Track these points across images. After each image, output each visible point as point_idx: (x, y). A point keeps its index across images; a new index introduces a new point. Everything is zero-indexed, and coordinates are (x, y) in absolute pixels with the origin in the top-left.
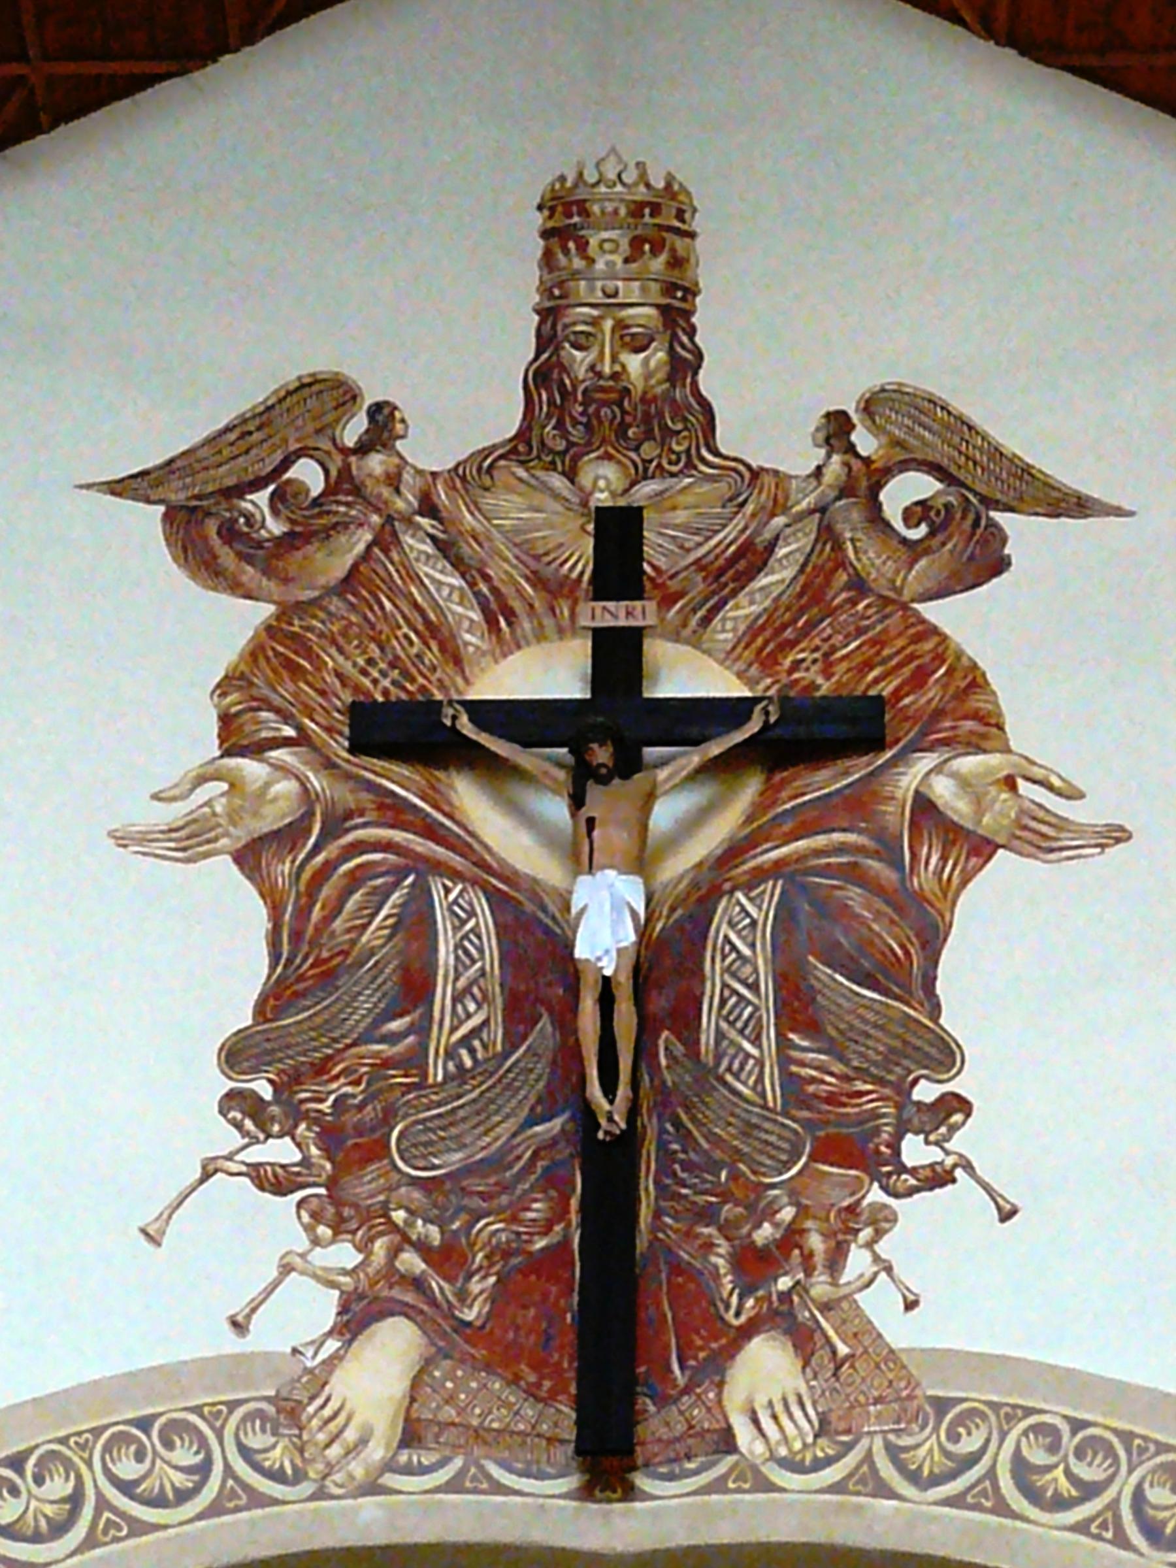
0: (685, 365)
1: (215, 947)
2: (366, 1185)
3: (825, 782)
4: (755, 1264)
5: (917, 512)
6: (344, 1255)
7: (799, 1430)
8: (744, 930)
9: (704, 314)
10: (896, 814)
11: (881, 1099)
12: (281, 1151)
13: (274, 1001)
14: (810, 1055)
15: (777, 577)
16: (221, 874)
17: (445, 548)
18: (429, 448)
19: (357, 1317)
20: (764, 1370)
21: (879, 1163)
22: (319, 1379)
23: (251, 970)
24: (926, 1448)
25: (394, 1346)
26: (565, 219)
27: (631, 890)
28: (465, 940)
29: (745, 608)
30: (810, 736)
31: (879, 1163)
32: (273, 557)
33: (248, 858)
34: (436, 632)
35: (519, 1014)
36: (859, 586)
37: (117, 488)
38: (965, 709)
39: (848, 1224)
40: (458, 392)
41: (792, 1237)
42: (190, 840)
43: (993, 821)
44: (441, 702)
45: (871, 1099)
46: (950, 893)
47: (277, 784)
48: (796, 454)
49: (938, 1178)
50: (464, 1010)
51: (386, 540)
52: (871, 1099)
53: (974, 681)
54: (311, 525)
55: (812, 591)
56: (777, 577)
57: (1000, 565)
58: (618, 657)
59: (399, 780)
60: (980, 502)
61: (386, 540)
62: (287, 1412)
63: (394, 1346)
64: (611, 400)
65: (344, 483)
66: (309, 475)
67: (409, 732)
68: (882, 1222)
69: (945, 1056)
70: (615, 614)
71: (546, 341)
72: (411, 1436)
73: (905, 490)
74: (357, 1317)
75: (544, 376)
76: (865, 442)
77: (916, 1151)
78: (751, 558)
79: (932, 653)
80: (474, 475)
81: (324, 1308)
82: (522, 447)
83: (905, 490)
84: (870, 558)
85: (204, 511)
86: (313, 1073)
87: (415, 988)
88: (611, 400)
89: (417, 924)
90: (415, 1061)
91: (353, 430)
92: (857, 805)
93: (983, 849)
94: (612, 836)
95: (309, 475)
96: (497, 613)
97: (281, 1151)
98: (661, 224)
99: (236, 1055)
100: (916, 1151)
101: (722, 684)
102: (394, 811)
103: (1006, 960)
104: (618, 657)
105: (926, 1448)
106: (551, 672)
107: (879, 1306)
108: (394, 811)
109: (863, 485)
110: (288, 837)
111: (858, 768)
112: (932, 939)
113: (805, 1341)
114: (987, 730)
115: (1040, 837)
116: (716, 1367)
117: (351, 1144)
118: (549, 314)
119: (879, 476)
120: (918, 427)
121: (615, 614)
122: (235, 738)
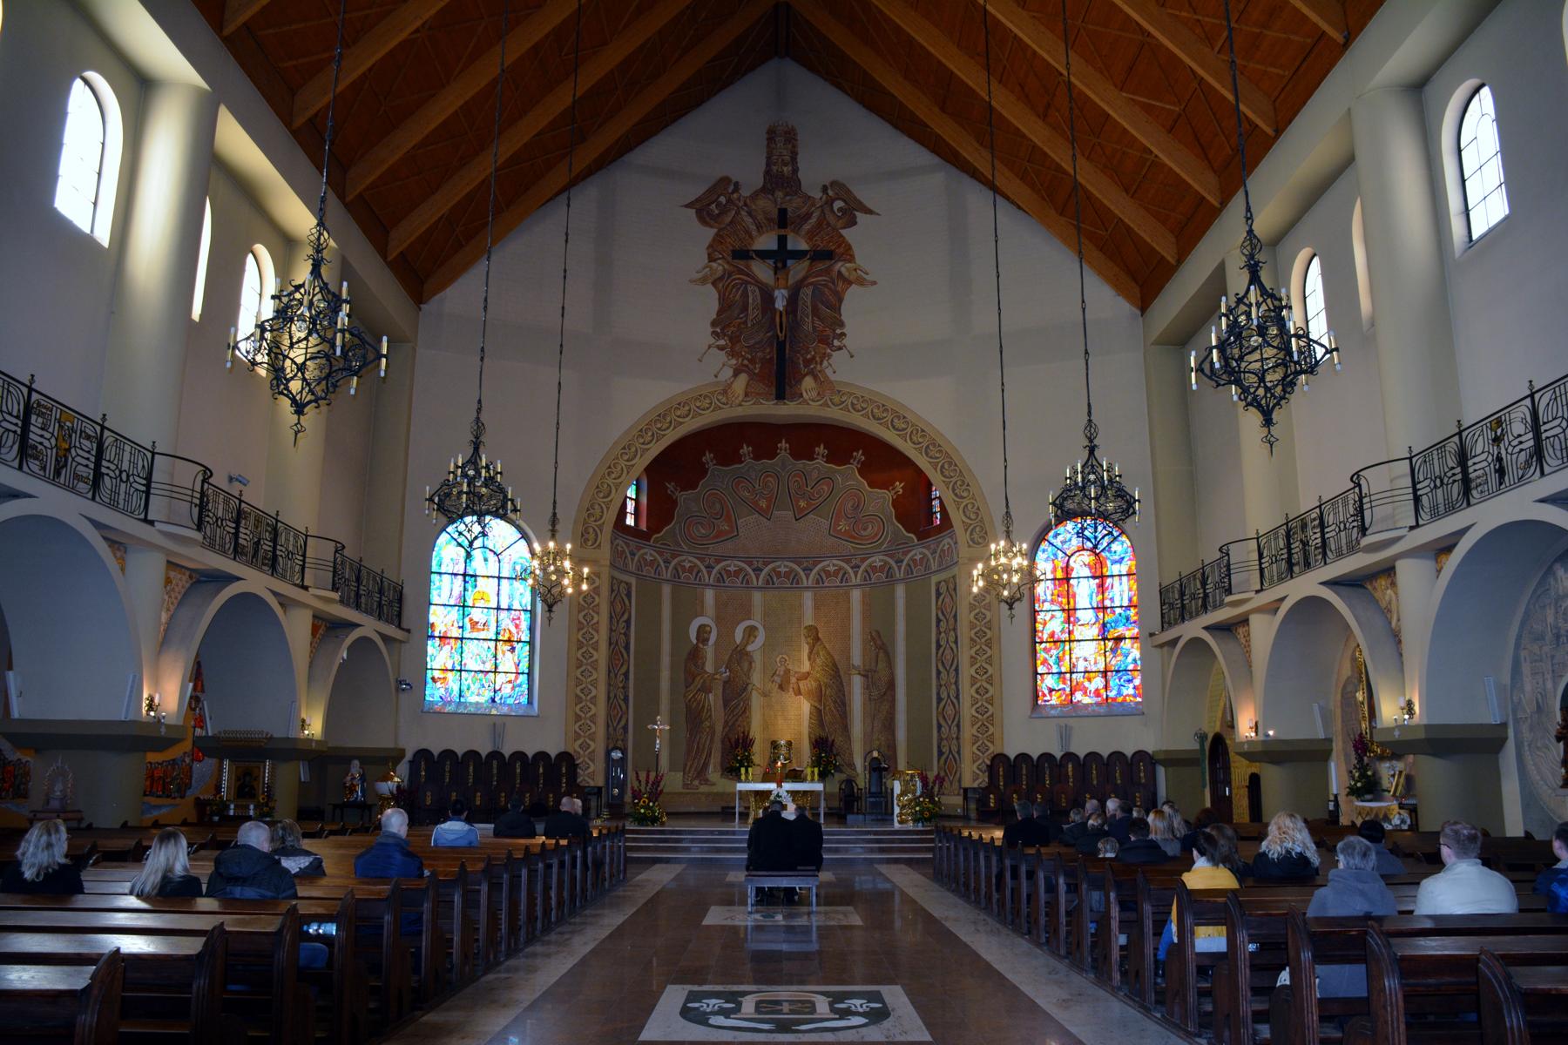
0: (795, 171)
1: (708, 302)
2: (737, 348)
3: (821, 266)
4: (807, 363)
5: (840, 209)
6: (734, 362)
7: (814, 394)
8: (806, 294)
9: (799, 158)
10: (834, 274)
11: (831, 331)
12: (722, 342)
13: (719, 313)
14: (818, 323)
15: (813, 220)
16: (710, 286)
17: (750, 214)
18: (745, 192)
19: (736, 373)
20: (808, 382)
21: (830, 345)
22: (730, 386)
23: (714, 306)
24: (836, 399)
25: (743, 378)
26: (771, 135)
27: (785, 292)
28: (754, 297)
29: (807, 227)
30: (822, 255)
31: (830, 345)
32: (716, 218)
33: (714, 284)
34: (748, 232)
35: (764, 312)
36: (828, 224)
37: (687, 206)
38: (848, 254)
39: (824, 356)
40: (749, 171)
41: (814, 358)
42: (703, 281)
43: (853, 277)
44: (1083, 807)
45: (828, 332)
46: (844, 291)
47: (719, 267)
48: (817, 194)
49: (840, 348)
50: (754, 313)
51: (738, 213)
52: (828, 332)
53: (849, 248)
54: (724, 210)
55: (819, 224)
56: (813, 220)
57: (855, 223)
58: (782, 240)
59: (741, 264)
60: (853, 210)
61: (738, 213)
62: (725, 392)
63: (743, 378)
64: (780, 180)
65: (729, 201)
66: (723, 199)
67: (743, 254)
68: (830, 356)
69: (842, 325)
70: (782, 232)
71: (768, 165)
72: (746, 395)
73: (838, 204)
74: (736, 373)
75: (767, 173)
76: (830, 193)
77: (836, 343)
78: (808, 216)
79: (842, 242)
80: (755, 196)
81: (730, 372)
82: (764, 190)
83: (838, 204)
84: (831, 219)
85: (704, 209)
86: (727, 325)
87: (745, 309)
88: (780, 180)
89: (745, 295)
90: (745, 323)
91: (731, 188)
92: (827, 271)
93: (850, 283)
94: (782, 282)
95: (723, 199)
96: (759, 227)
97: (722, 342)
98: (790, 136)
99: (713, 324)
100: (836, 343)
101: (804, 246)
102: (741, 271)
103: (854, 305)
104: (782, 240)
105: (836, 399)
106: (767, 242)
107: (829, 372)
108: (741, 271)
109: (830, 202)
110: (721, 279)
111: (828, 263)
112: (840, 300)
113: (815, 378)
114: (851, 259)
115: (861, 282)
116: (799, 381)
117: (734, 340)
118: (768, 158)
119: (833, 201)
120: (837, 189)
121: (782, 232)
122: (711, 259)
